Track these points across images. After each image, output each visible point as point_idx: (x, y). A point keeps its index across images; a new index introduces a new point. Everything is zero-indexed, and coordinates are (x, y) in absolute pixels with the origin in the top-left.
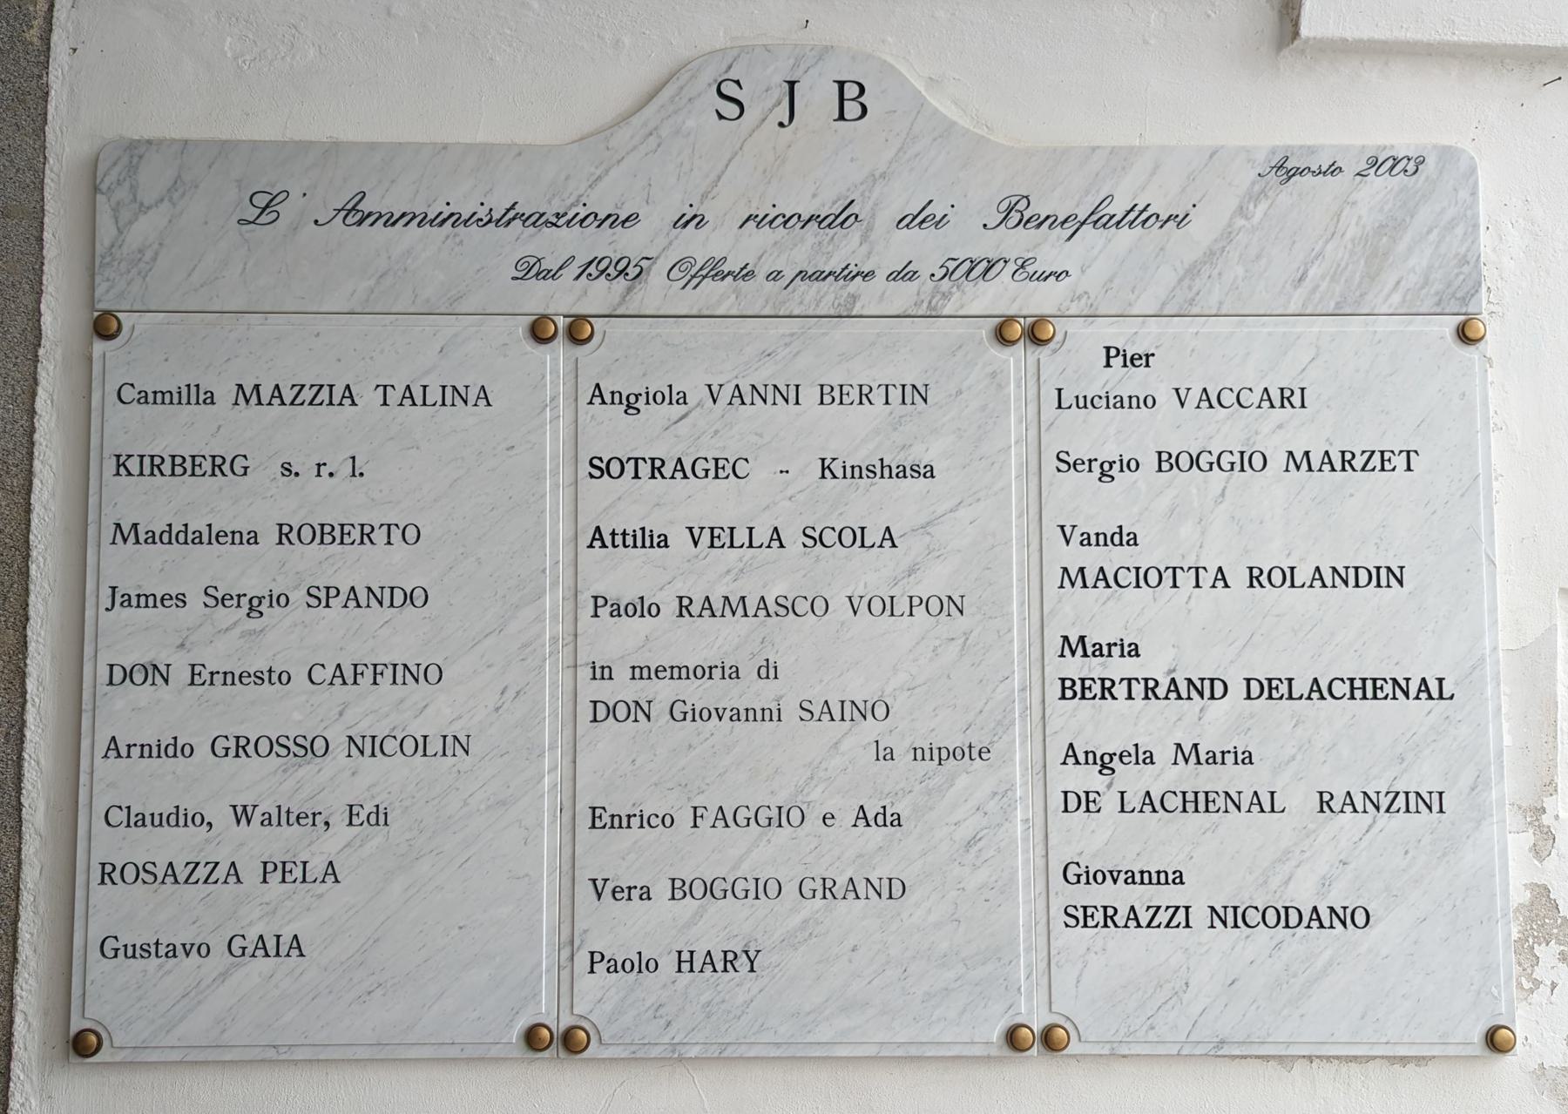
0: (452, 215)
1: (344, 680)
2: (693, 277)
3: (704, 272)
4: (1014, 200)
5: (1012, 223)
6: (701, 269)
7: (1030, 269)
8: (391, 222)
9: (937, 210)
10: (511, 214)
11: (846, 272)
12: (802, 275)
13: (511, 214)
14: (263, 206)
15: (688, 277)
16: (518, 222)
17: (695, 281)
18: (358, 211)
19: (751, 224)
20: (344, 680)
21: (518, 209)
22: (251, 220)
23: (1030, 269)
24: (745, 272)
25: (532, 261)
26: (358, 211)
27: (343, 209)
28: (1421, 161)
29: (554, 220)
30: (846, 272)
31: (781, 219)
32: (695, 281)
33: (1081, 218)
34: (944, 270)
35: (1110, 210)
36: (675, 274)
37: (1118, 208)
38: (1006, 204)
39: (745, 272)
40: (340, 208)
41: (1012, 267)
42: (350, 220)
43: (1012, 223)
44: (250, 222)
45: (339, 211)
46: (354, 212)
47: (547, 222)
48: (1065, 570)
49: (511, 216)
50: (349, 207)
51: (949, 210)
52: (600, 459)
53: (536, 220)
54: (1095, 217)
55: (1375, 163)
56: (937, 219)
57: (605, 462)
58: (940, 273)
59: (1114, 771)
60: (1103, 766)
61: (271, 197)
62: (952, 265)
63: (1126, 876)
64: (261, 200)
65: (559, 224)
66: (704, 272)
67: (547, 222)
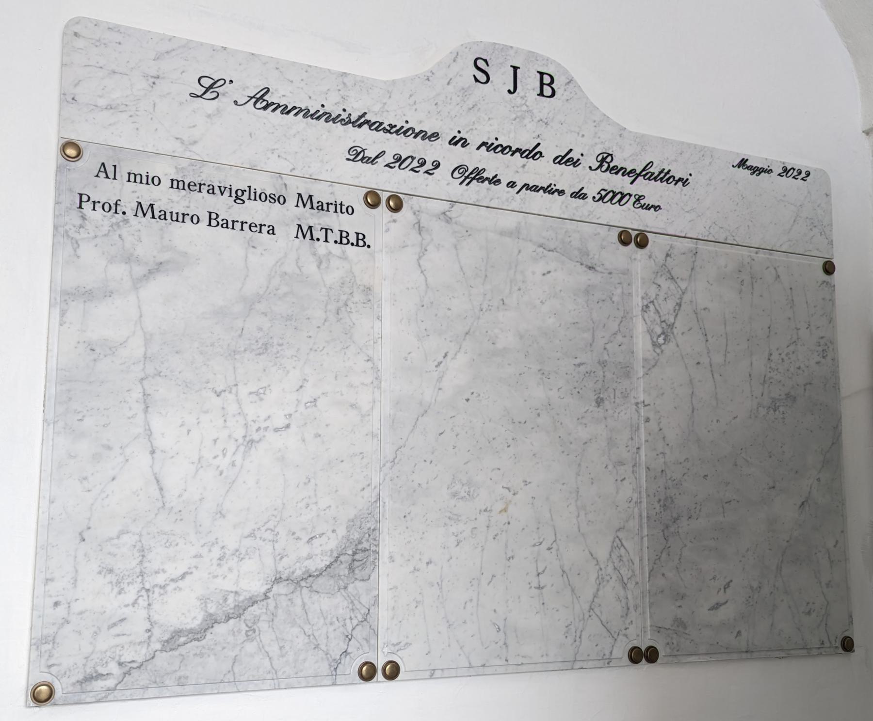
0: (461, 139)
1: (107, 174)
2: (467, 178)
3: (473, 176)
4: (605, 155)
5: (604, 168)
6: (471, 173)
7: (642, 202)
8: (286, 111)
9: (575, 155)
10: (362, 120)
11: (550, 189)
12: (526, 186)
13: (362, 120)
14: (207, 86)
15: (463, 178)
16: (366, 126)
17: (468, 180)
18: (264, 100)
19: (484, 148)
20: (107, 174)
21: (367, 117)
22: (199, 95)
23: (642, 202)
24: (495, 179)
25: (359, 150)
26: (264, 100)
27: (254, 97)
28: (808, 174)
29: (388, 128)
30: (550, 189)
31: (500, 149)
32: (468, 180)
33: (638, 172)
34: (600, 195)
35: (651, 170)
36: (456, 174)
37: (655, 170)
38: (600, 158)
39: (495, 179)
40: (252, 96)
41: (633, 199)
42: (258, 105)
43: (604, 168)
44: (198, 96)
45: (252, 98)
46: (261, 101)
47: (384, 128)
48: (300, 195)
49: (361, 122)
50: (258, 96)
51: (580, 157)
52: (270, 202)
53: (376, 126)
54: (644, 173)
55: (786, 171)
56: (575, 161)
57: (268, 200)
58: (598, 197)
59: (244, 202)
60: (237, 197)
61: (213, 81)
62: (603, 193)
63: (208, 188)
64: (207, 82)
65: (392, 131)
66: (473, 176)
67: (384, 128)
